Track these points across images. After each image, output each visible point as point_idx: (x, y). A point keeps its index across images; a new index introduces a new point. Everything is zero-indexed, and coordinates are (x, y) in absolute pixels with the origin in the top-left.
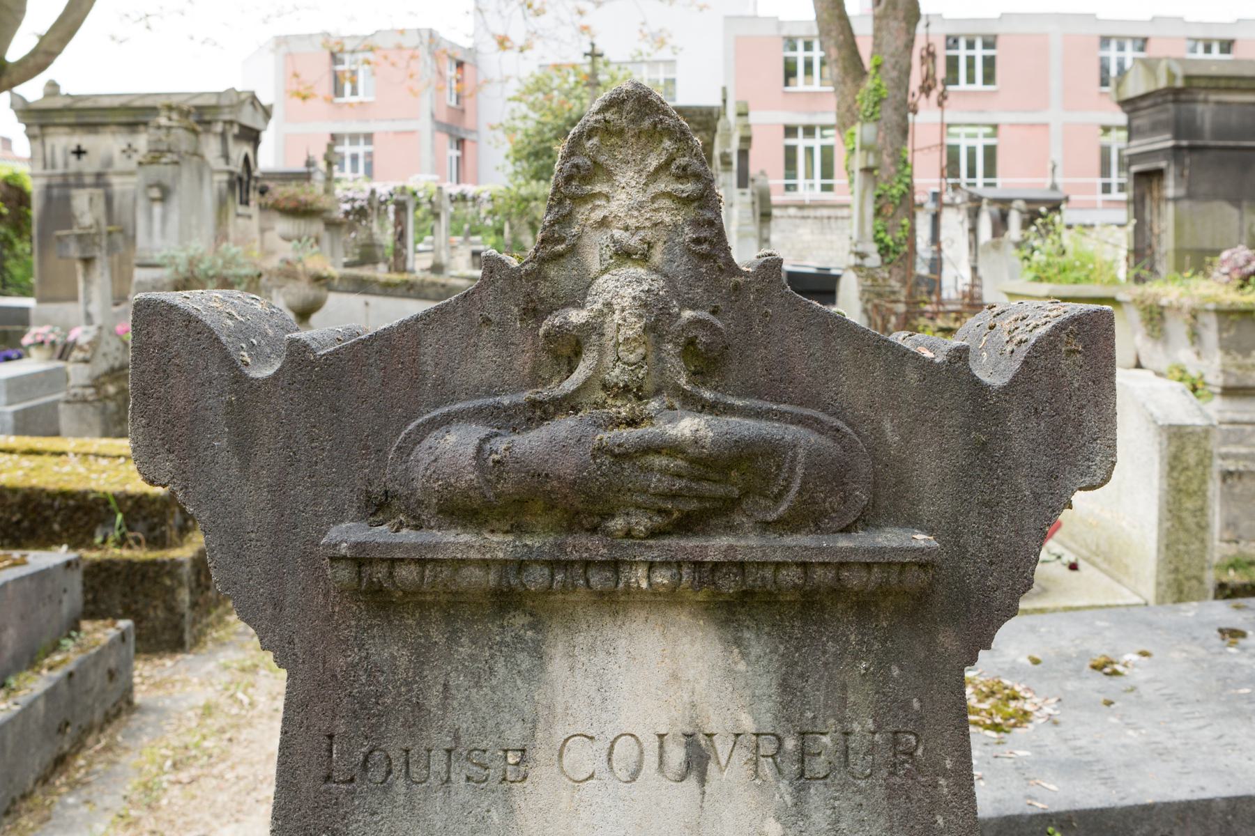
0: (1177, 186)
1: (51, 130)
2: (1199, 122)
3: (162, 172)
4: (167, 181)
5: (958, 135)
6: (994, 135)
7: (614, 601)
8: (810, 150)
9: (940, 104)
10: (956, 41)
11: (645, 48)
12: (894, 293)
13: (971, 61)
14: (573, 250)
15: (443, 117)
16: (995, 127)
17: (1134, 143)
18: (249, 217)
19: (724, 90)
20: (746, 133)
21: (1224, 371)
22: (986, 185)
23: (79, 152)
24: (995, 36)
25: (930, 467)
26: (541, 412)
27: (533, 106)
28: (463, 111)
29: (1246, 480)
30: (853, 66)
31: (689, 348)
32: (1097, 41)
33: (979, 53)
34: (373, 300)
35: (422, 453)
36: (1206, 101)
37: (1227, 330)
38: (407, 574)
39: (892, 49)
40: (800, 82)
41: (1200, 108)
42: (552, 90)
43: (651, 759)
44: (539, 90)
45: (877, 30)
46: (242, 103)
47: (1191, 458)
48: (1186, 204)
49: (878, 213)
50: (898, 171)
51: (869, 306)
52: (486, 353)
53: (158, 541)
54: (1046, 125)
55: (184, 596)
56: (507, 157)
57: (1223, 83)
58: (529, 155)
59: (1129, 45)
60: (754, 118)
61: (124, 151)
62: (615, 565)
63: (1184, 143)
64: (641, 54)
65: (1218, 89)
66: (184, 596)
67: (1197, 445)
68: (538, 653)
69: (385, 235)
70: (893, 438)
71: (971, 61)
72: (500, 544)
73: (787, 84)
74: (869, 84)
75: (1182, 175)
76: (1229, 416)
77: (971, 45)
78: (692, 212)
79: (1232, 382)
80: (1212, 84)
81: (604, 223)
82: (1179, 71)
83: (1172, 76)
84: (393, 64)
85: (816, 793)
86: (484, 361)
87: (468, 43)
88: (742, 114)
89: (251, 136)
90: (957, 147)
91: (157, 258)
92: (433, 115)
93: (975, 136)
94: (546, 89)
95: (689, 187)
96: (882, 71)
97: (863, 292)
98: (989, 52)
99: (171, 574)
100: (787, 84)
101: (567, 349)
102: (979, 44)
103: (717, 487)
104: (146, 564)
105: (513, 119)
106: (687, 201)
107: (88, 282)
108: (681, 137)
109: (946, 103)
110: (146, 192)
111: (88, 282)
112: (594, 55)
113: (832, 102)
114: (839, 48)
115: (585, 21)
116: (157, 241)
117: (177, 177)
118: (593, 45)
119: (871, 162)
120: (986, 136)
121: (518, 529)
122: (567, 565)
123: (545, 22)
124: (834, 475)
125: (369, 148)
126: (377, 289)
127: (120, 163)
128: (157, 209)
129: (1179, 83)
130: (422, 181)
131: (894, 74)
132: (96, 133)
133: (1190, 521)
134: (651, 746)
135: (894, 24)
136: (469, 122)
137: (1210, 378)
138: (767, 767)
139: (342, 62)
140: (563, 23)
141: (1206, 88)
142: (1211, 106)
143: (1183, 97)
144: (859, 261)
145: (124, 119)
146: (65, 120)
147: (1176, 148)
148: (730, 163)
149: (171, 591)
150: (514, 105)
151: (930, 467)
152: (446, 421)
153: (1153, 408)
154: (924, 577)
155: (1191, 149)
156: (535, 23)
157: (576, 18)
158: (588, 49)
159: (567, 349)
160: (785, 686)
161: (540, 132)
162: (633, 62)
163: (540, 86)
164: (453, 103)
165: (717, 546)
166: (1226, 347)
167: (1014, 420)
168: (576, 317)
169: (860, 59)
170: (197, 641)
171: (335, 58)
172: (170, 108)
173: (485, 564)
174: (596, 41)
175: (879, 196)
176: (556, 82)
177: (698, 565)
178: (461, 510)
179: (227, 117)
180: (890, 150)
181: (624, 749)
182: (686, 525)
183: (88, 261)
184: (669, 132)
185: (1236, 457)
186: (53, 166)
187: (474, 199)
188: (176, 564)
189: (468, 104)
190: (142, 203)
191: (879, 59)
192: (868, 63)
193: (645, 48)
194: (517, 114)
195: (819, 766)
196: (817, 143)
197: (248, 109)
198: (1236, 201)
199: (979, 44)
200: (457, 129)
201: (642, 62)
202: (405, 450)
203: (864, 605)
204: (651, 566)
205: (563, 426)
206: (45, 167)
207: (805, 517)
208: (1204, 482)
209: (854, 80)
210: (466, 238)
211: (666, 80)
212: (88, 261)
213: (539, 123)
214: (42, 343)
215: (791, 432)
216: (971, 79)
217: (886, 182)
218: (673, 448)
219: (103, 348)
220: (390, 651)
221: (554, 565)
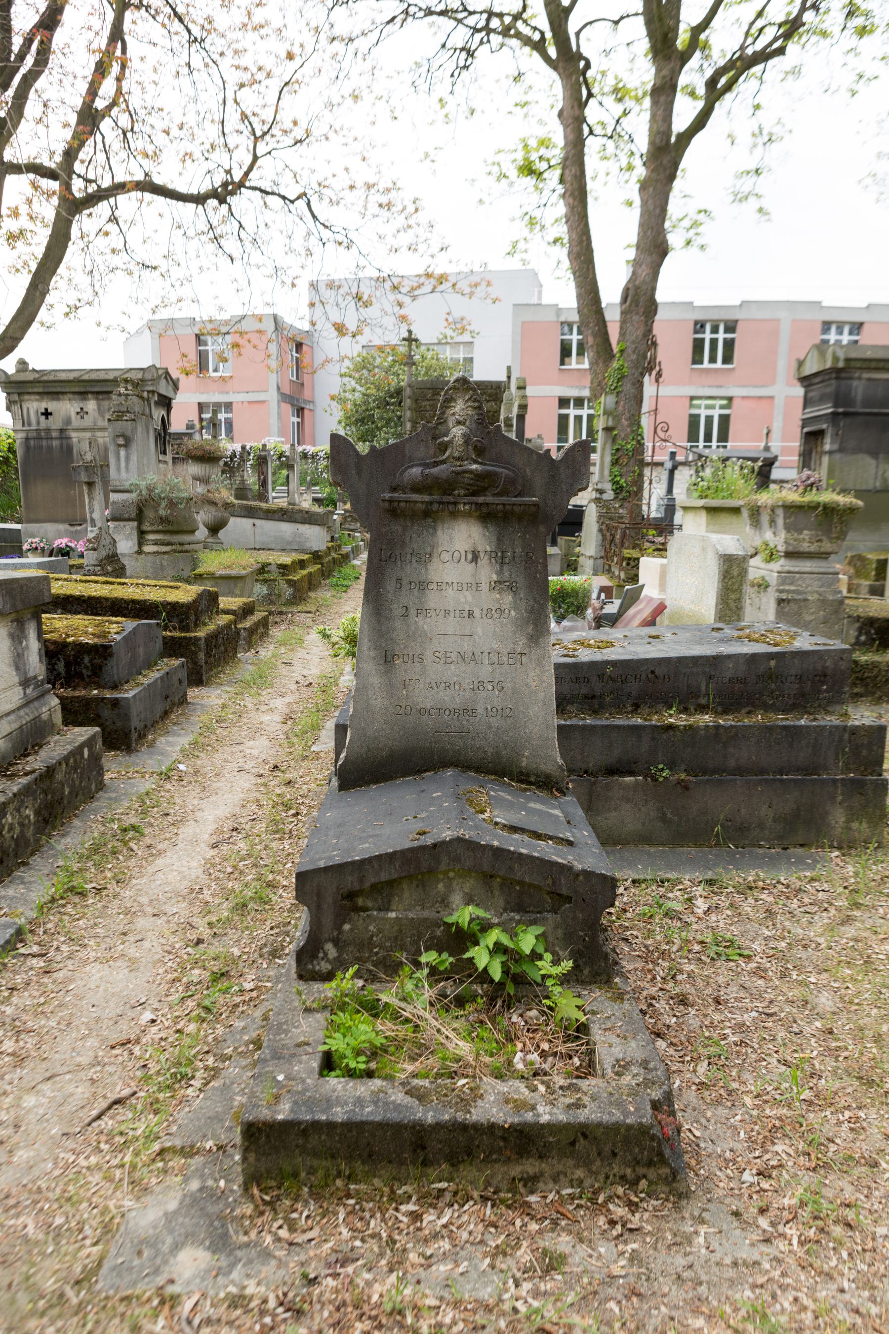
0: (831, 443)
1: (26, 397)
2: (853, 394)
3: (124, 426)
4: (128, 433)
5: (699, 407)
6: (728, 406)
7: (455, 515)
8: (579, 419)
9: (657, 381)
10: (703, 326)
11: (449, 333)
12: (622, 518)
13: (714, 342)
14: (445, 421)
15: (287, 390)
16: (730, 399)
17: (807, 411)
18: (165, 462)
19: (509, 368)
20: (523, 402)
21: (786, 542)
22: (705, 447)
23: (47, 414)
24: (736, 321)
25: (539, 481)
26: (436, 464)
27: (359, 381)
28: (302, 385)
29: (792, 604)
30: (604, 351)
31: (475, 448)
32: (819, 327)
33: (721, 336)
34: (258, 522)
35: (406, 474)
36: (860, 378)
37: (790, 517)
38: (402, 504)
39: (633, 338)
40: (573, 363)
41: (855, 383)
42: (374, 367)
43: (463, 557)
44: (364, 368)
45: (623, 322)
46: (159, 377)
47: (735, 572)
48: (838, 456)
49: (615, 463)
50: (633, 431)
51: (604, 527)
52: (422, 449)
53: (185, 629)
54: (772, 398)
55: (202, 656)
56: (340, 422)
57: (873, 365)
58: (357, 421)
59: (846, 330)
60: (530, 391)
61: (78, 413)
62: (455, 503)
63: (841, 410)
64: (446, 337)
65: (869, 369)
66: (202, 656)
67: (739, 566)
68: (435, 529)
69: (251, 479)
70: (529, 473)
71: (714, 342)
72: (426, 498)
73: (562, 363)
74: (615, 365)
75: (837, 434)
76: (787, 568)
77: (715, 330)
78: (477, 411)
79: (791, 549)
80: (866, 365)
81: (453, 414)
82: (841, 355)
83: (836, 359)
84: (255, 347)
85: (506, 568)
86: (421, 452)
87: (306, 327)
88: (521, 388)
89: (166, 403)
90: (699, 416)
91: (127, 485)
92: (278, 388)
93: (712, 407)
94: (371, 367)
95: (476, 404)
96: (625, 355)
97: (600, 517)
98: (729, 336)
99: (194, 644)
100: (562, 363)
101: (444, 447)
102: (722, 328)
103: (481, 484)
104: (180, 638)
105: (345, 391)
106: (475, 408)
107: (91, 498)
108: (474, 390)
109: (661, 380)
110: (114, 440)
111: (91, 498)
112: (410, 340)
113: (587, 380)
114: (595, 336)
115: (403, 312)
116: (124, 474)
117: (134, 430)
118: (410, 332)
119: (610, 423)
120: (722, 407)
121: (430, 494)
122: (443, 503)
123: (372, 312)
124: (512, 482)
125: (229, 415)
126: (261, 514)
127: (76, 422)
128: (123, 452)
129: (841, 365)
130: (276, 442)
131: (634, 357)
132: (58, 399)
133: (733, 605)
134: (463, 554)
135: (636, 318)
136: (307, 394)
137: (780, 548)
138: (493, 561)
139: (206, 344)
140: (386, 313)
141: (860, 368)
142: (863, 382)
143: (843, 375)
144: (598, 496)
145: (77, 390)
146: (36, 390)
147: (834, 414)
148: (512, 426)
149: (196, 653)
150: (346, 380)
151: (539, 481)
152: (412, 466)
153: (718, 547)
154: (535, 509)
155: (845, 414)
156: (365, 313)
157: (397, 309)
158: (406, 335)
159: (444, 447)
160: (498, 539)
161: (366, 403)
162: (439, 343)
163: (364, 364)
164: (294, 379)
165: (481, 499)
166: (788, 528)
167: (562, 468)
168: (446, 439)
169: (610, 345)
170: (207, 683)
171: (199, 339)
172: (126, 381)
173: (422, 502)
174: (412, 328)
175: (618, 450)
176: (378, 361)
177: (476, 504)
178: (416, 488)
179: (150, 388)
180: (627, 415)
181: (456, 554)
182: (474, 494)
183: (90, 484)
184: (471, 389)
185: (788, 591)
186: (29, 424)
187: (313, 457)
188: (198, 639)
189: (306, 379)
190: (112, 448)
191: (623, 345)
192: (616, 348)
193: (449, 333)
194: (349, 387)
195: (507, 560)
196: (585, 412)
197: (163, 382)
198: (874, 454)
199: (722, 328)
200: (298, 400)
201: (447, 343)
202: (401, 474)
203: (520, 519)
204: (465, 504)
205: (443, 467)
206: (23, 425)
207: (504, 493)
208: (741, 585)
209: (605, 361)
210: (308, 488)
211: (465, 359)
212: (90, 484)
213: (364, 395)
214: (36, 548)
215: (501, 470)
216: (713, 360)
217: (623, 439)
218: (471, 472)
219: (103, 542)
220: (397, 528)
221: (440, 503)
